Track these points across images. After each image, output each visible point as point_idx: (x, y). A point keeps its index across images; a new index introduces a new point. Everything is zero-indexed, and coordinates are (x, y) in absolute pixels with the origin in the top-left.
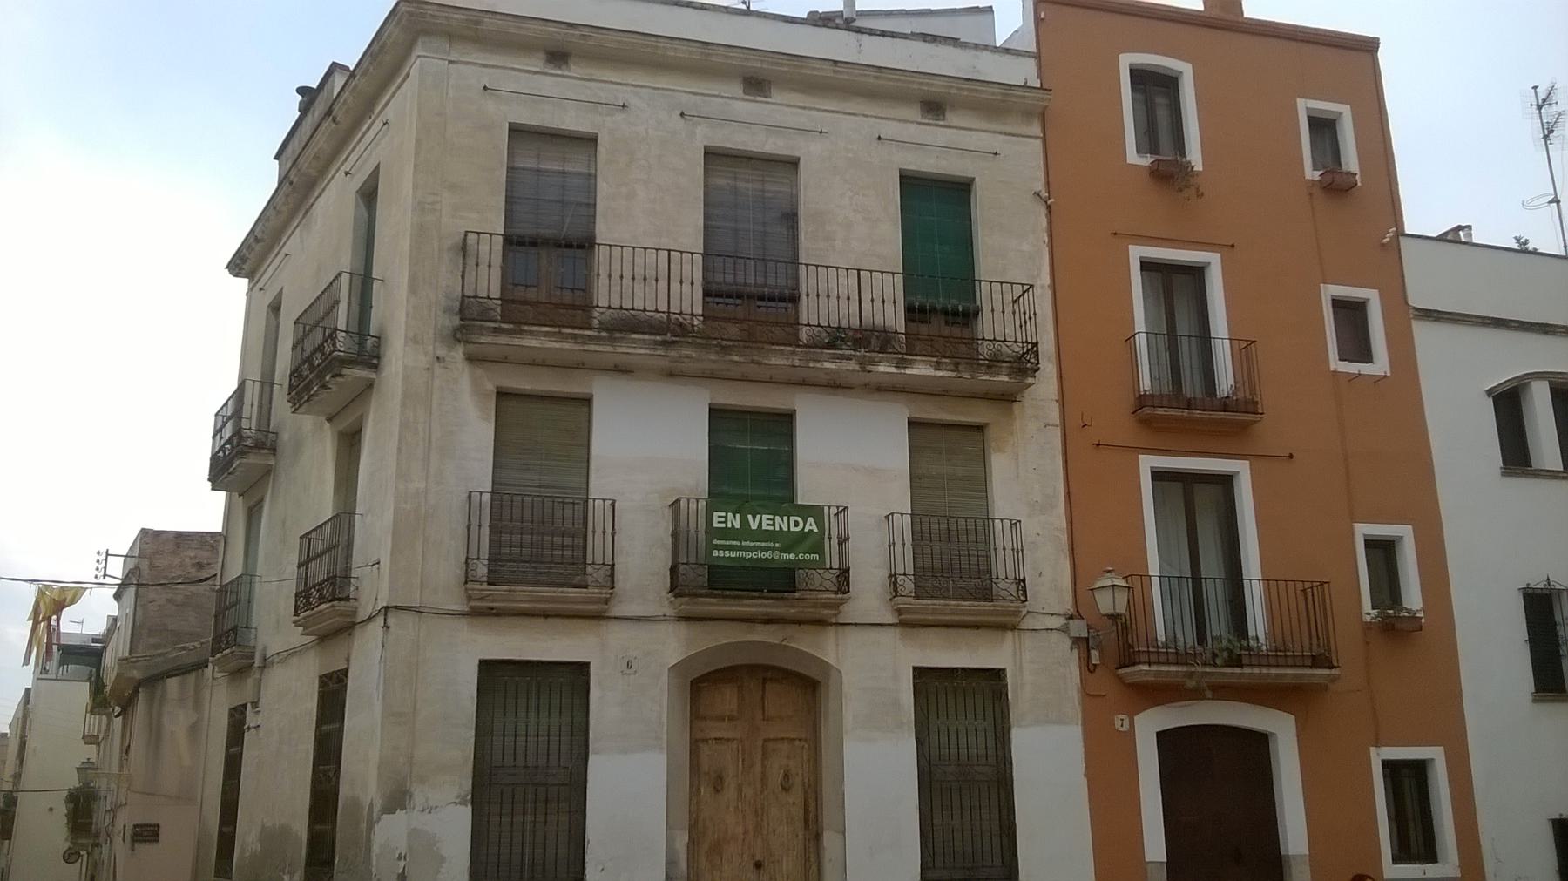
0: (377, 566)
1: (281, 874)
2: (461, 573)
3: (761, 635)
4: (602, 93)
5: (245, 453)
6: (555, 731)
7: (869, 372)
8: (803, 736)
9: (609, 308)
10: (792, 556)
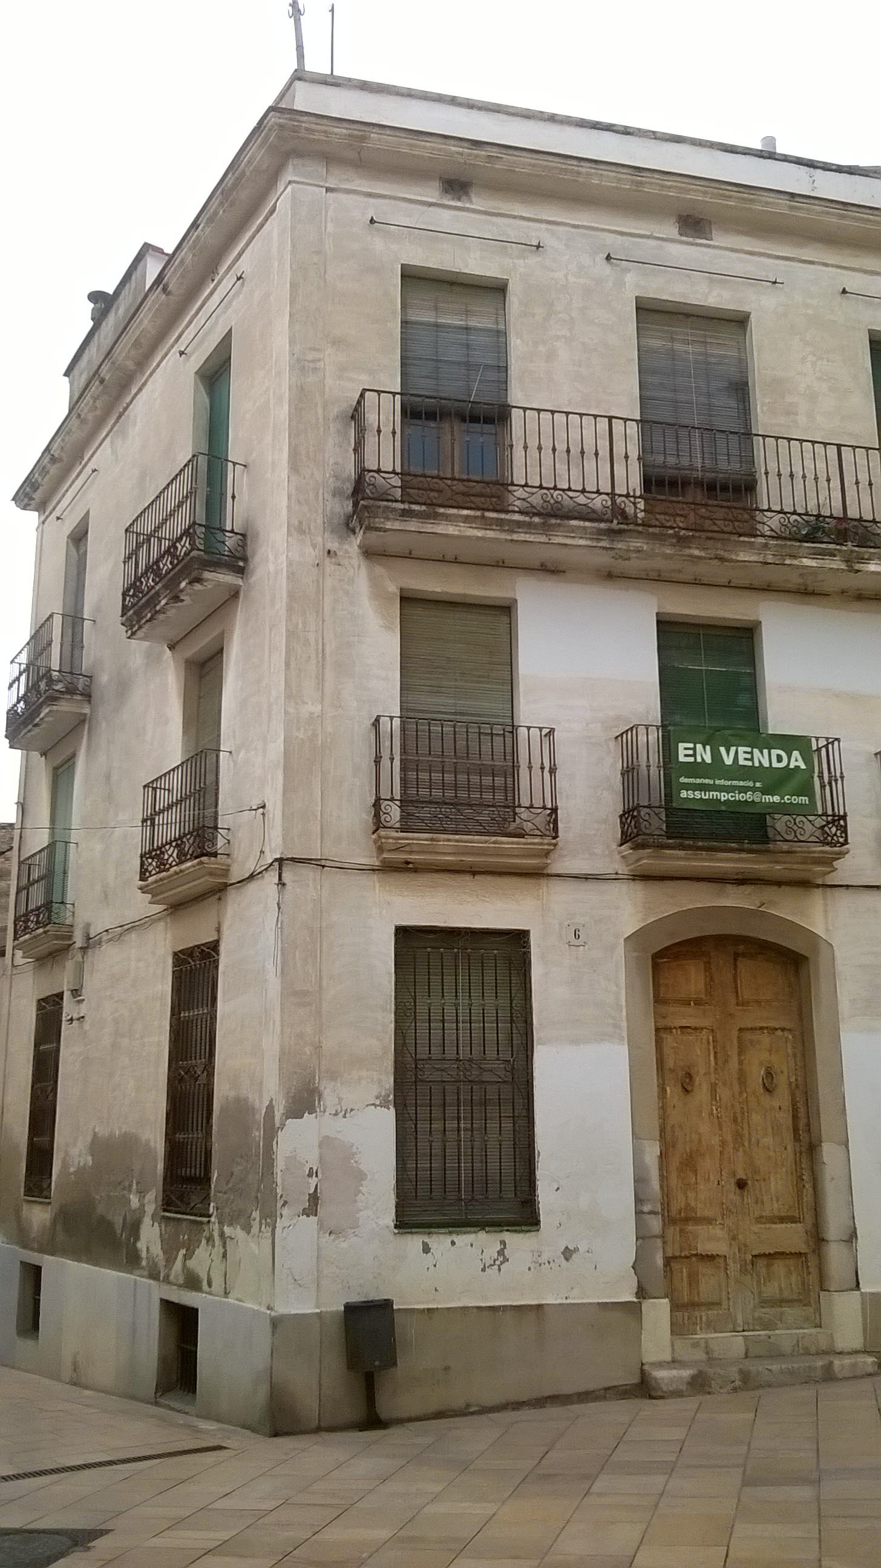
0: (261, 810)
1: (125, 1192)
2: (368, 817)
3: (733, 899)
4: (514, 230)
5: (56, 699)
6: (490, 1015)
7: (858, 571)
8: (787, 1025)
9: (541, 487)
10: (776, 799)
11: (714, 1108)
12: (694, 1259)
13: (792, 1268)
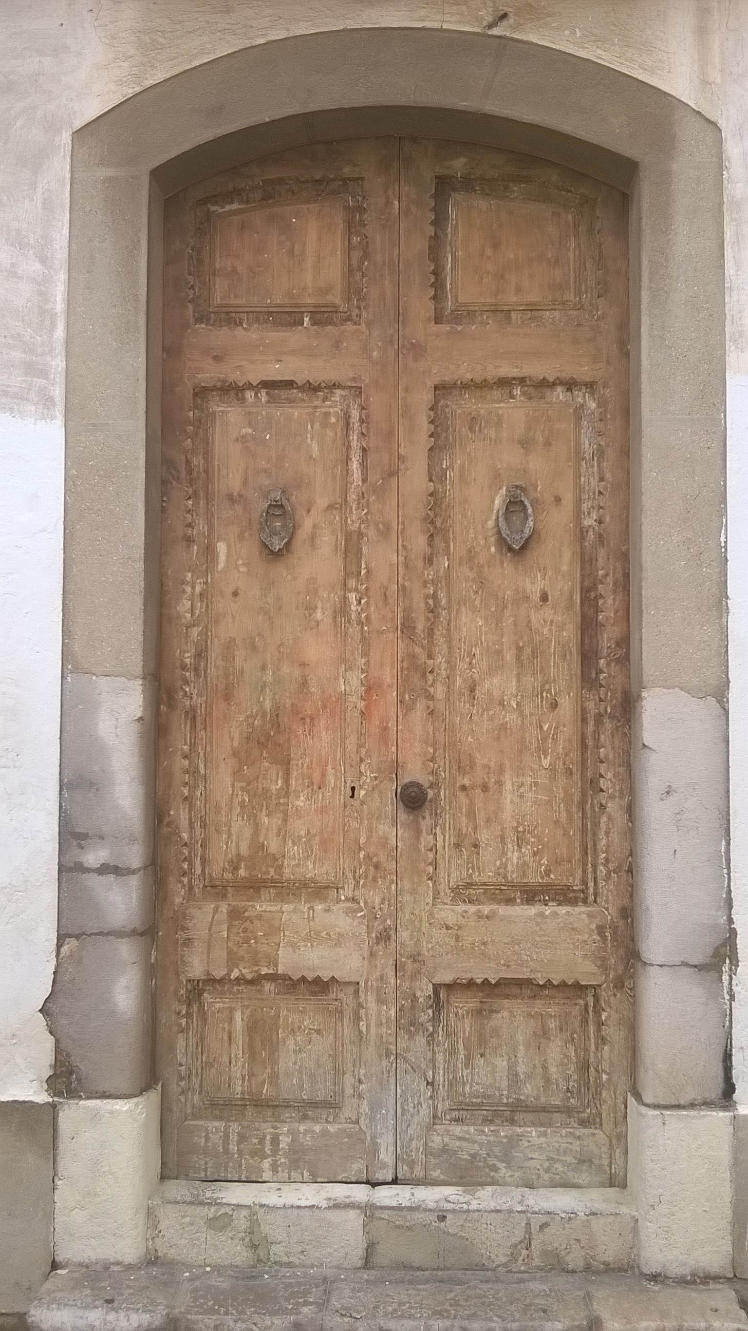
8: (584, 372)
11: (352, 597)
12: (268, 986)
13: (552, 1024)
